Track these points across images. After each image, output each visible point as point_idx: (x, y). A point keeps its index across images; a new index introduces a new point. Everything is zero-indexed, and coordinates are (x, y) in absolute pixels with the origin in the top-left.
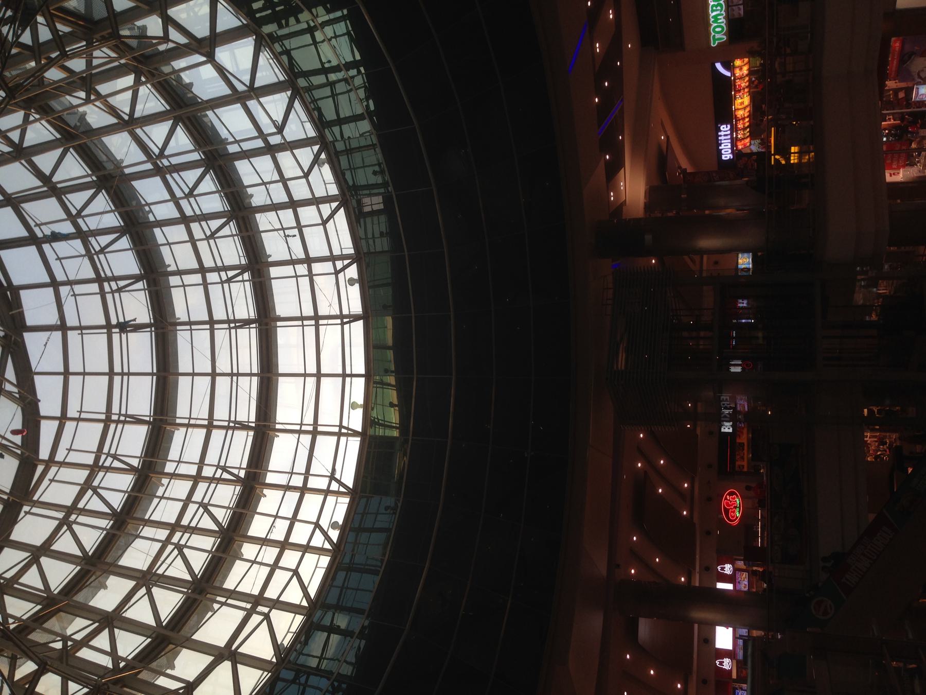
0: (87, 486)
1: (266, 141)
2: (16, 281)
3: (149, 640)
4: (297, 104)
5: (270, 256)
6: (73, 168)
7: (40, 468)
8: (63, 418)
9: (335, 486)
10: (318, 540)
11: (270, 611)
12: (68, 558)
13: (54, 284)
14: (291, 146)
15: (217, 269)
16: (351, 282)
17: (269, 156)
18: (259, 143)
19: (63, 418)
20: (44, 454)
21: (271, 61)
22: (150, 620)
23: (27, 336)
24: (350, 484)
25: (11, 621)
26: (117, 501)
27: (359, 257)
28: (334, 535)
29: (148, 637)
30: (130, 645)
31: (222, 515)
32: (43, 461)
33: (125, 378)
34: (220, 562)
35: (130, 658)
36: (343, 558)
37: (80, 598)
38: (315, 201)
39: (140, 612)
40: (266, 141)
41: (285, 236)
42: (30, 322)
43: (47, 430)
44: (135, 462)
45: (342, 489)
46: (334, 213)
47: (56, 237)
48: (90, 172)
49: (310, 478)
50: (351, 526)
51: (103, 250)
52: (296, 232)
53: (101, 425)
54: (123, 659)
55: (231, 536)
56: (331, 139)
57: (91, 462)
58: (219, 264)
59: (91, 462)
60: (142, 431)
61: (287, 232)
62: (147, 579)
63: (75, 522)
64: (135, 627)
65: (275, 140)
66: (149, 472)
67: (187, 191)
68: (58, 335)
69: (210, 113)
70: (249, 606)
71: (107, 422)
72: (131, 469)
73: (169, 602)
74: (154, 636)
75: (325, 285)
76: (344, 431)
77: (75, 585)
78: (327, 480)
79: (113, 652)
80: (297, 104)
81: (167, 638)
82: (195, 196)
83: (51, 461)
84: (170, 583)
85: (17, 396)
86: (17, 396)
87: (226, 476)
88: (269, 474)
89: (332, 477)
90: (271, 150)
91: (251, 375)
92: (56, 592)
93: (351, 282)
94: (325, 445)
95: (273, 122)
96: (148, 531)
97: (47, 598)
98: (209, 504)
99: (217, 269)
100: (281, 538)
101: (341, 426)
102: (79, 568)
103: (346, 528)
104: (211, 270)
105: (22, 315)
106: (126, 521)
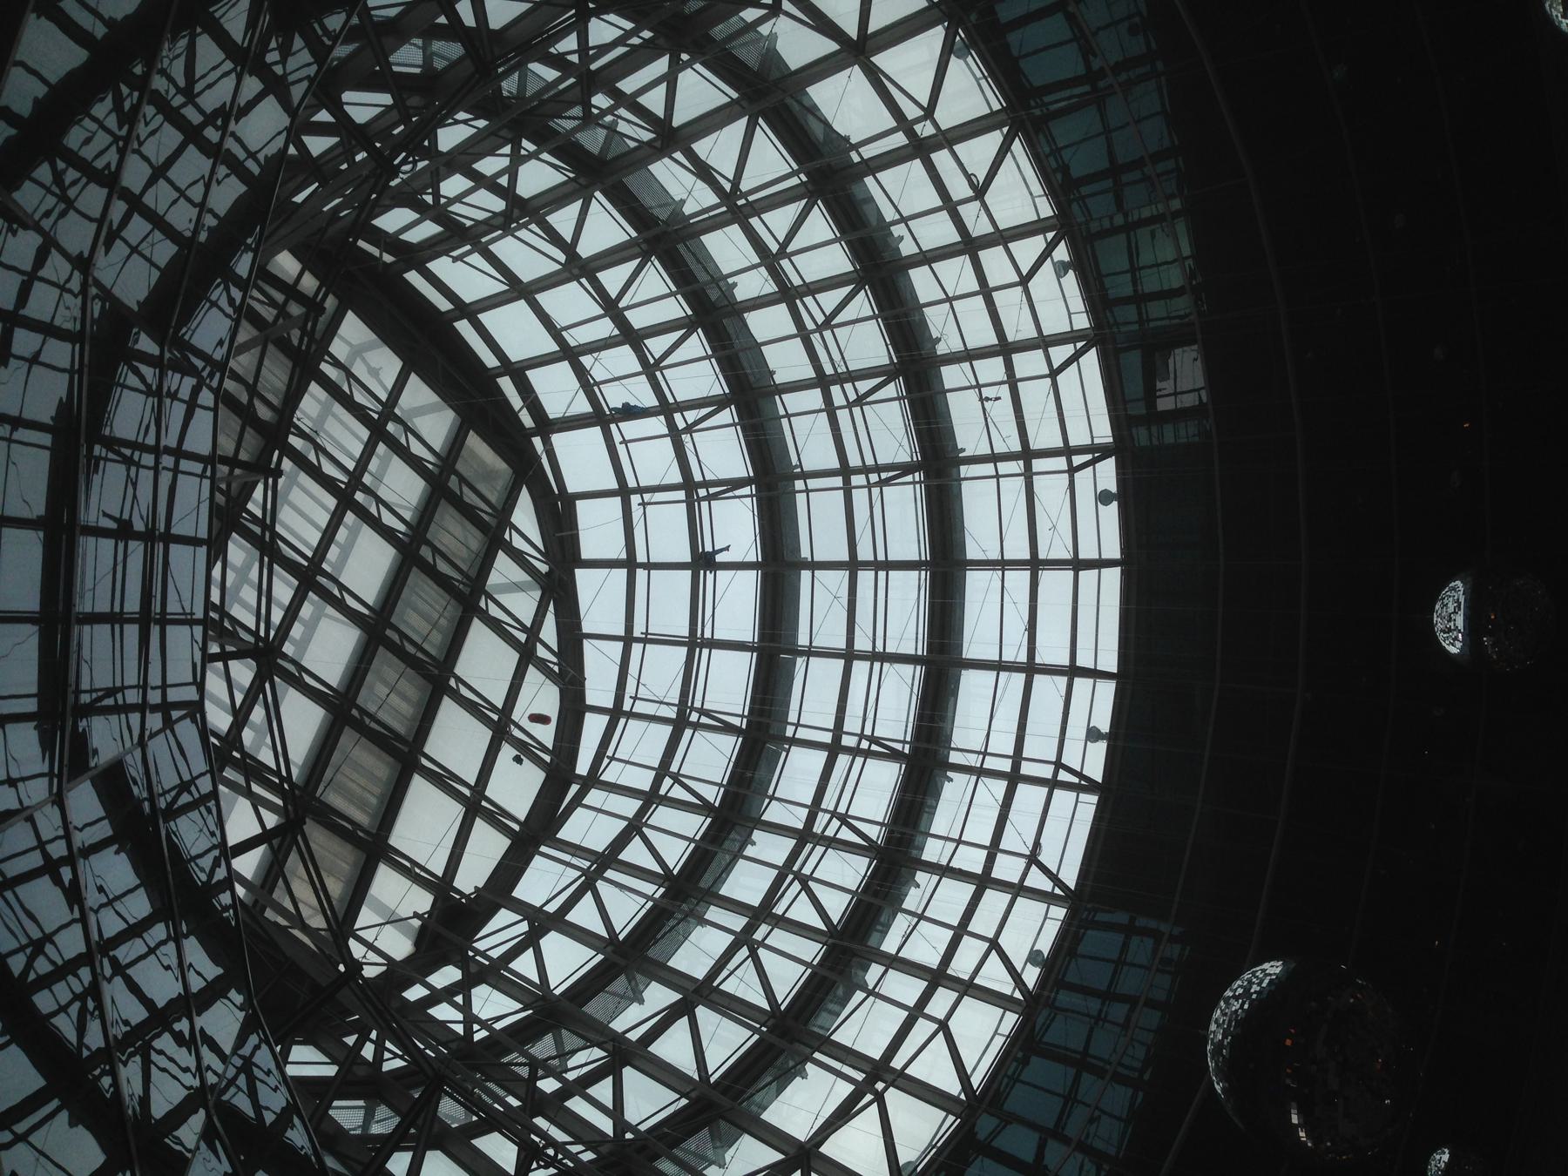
0: (634, 827)
1: (910, 133)
2: (572, 488)
3: (684, 1102)
4: (1017, 146)
5: (963, 450)
6: (604, 228)
7: (574, 788)
8: (616, 713)
9: (1037, 880)
10: (995, 977)
11: (885, 1089)
12: (577, 933)
13: (624, 492)
14: (1003, 237)
15: (865, 470)
16: (1104, 498)
17: (856, 70)
18: (899, 139)
19: (616, 713)
20: (582, 768)
21: (983, 82)
22: (688, 1066)
23: (579, 572)
24: (1070, 877)
25: (476, 1027)
26: (675, 854)
27: (1120, 448)
28: (1031, 976)
29: (683, 1095)
30: (647, 1102)
31: (837, 905)
32: (580, 777)
33: (859, 760)
34: (659, 925)
35: (643, 1128)
36: (1038, 1013)
37: (594, 1008)
38: (1044, 342)
39: (674, 1048)
40: (910, 133)
41: (981, 399)
42: (586, 554)
43: (594, 727)
44: (712, 795)
45: (1057, 891)
46: (1075, 358)
47: (630, 412)
48: (674, 289)
49: (1000, 857)
50: (1058, 963)
51: (690, 429)
52: (1005, 391)
53: (667, 730)
54: (633, 1129)
55: (849, 949)
56: (1081, 219)
57: (647, 787)
58: (870, 461)
59: (647, 787)
60: (728, 745)
61: (986, 392)
62: (699, 994)
63: (762, 944)
64: (663, 1073)
65: (925, 130)
66: (734, 815)
67: (820, 319)
68: (622, 574)
69: (869, 181)
70: (860, 1076)
71: (680, 724)
72: (703, 807)
73: (726, 1042)
74: (693, 1095)
75: (1051, 489)
76: (1064, 776)
77: (589, 985)
78: (1022, 862)
79: (616, 1111)
80: (1017, 146)
81: (721, 1105)
82: (832, 328)
83: (593, 780)
84: (732, 1007)
85: (556, 669)
86: (556, 669)
87: (846, 835)
88: (930, 842)
89: (1033, 859)
90: (920, 149)
91: (815, 566)
92: (557, 992)
93: (1104, 498)
94: (1029, 798)
95: (969, 177)
96: (714, 913)
97: (543, 998)
98: (811, 877)
99: (865, 470)
100: (932, 960)
101: (1059, 765)
102: (600, 957)
103: (1055, 964)
104: (857, 471)
105: (575, 540)
106: (687, 892)
